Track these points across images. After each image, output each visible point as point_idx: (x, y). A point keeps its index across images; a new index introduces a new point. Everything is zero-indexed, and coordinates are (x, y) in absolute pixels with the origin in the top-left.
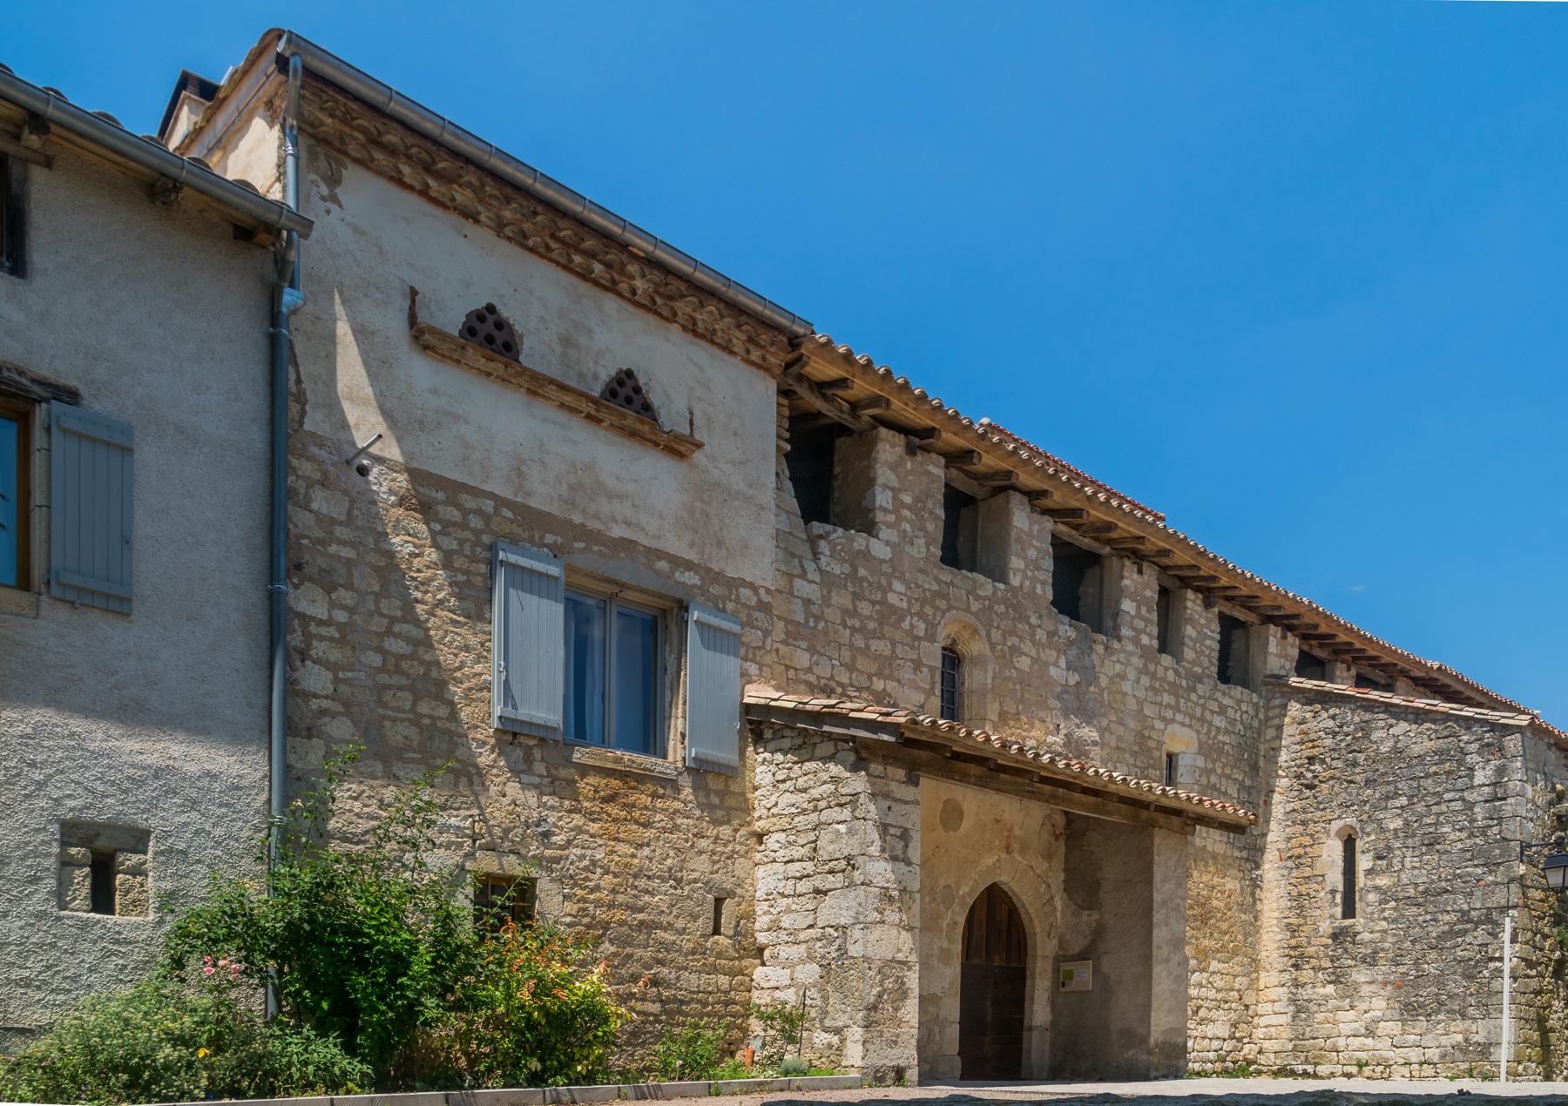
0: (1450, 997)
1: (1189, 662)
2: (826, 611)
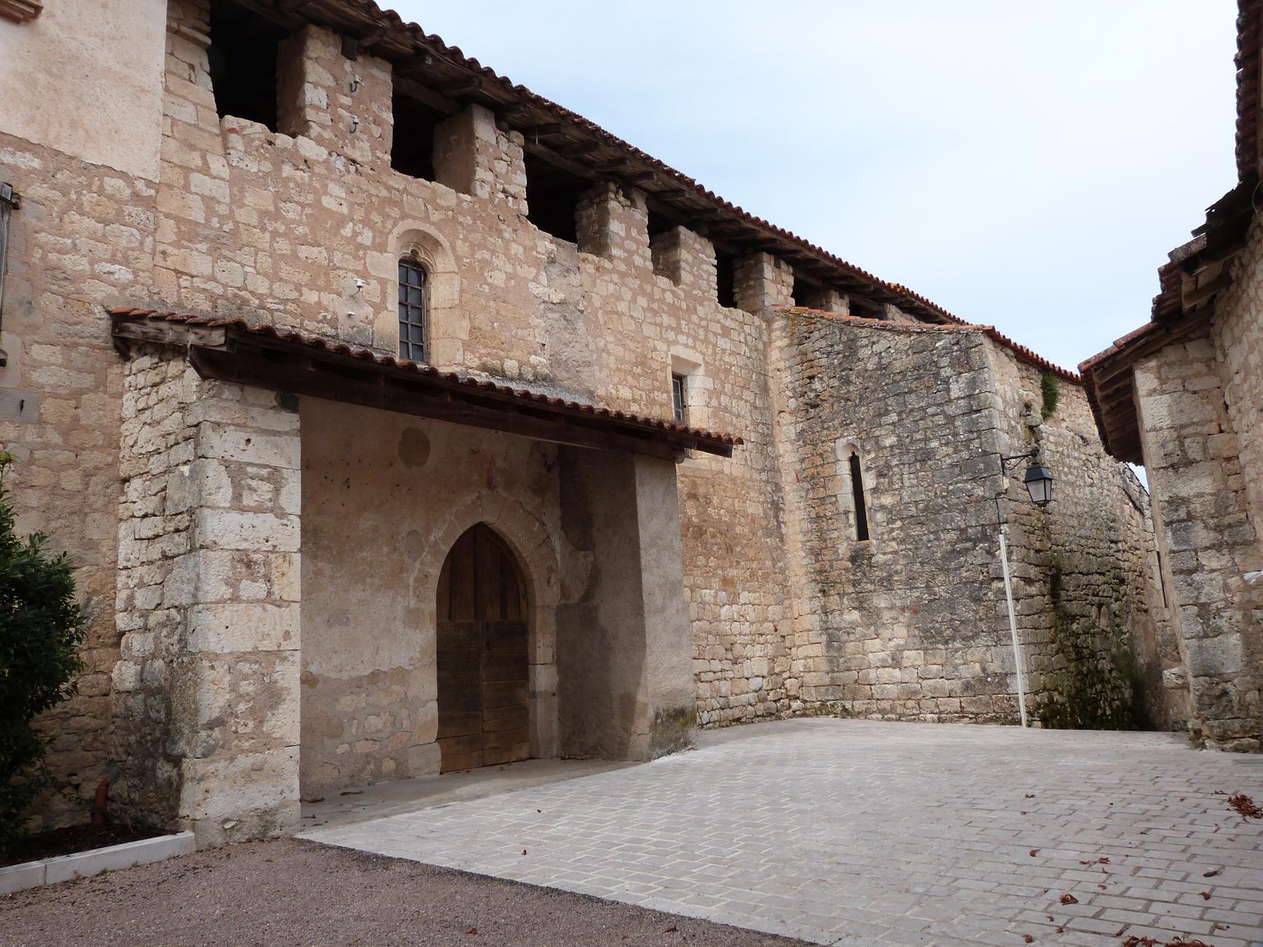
0: (962, 622)
1: (687, 285)
2: (237, 211)
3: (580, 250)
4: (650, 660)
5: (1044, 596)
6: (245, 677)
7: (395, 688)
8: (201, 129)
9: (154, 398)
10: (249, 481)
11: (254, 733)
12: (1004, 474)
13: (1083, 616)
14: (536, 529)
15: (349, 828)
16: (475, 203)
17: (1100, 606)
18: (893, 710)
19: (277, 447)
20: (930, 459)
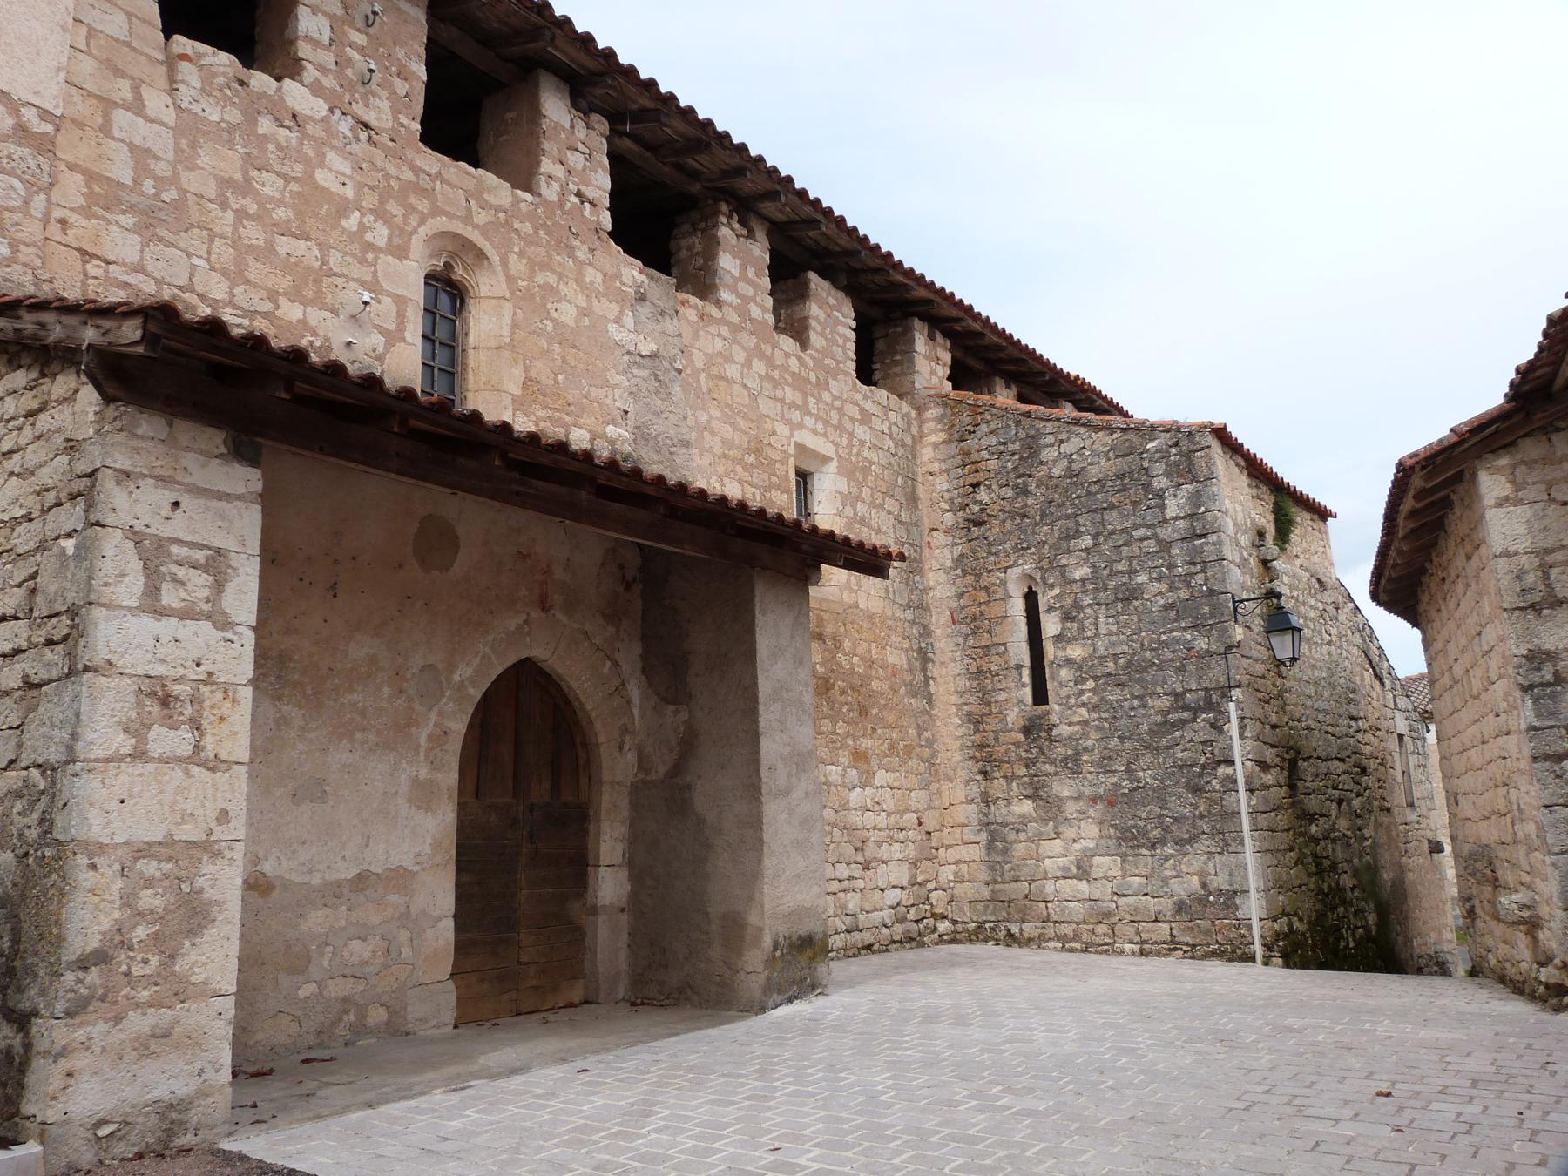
0: (1175, 820)
1: (817, 351)
2: (184, 175)
3: (679, 288)
4: (769, 863)
5: (1281, 786)
6: (149, 883)
7: (393, 898)
8: (134, 49)
9: (28, 433)
10: (174, 568)
11: (159, 975)
12: (1236, 621)
13: (1323, 815)
14: (606, 670)
15: (309, 1127)
16: (537, 205)
17: (1340, 802)
18: (1076, 937)
19: (223, 517)
20: (1136, 599)
